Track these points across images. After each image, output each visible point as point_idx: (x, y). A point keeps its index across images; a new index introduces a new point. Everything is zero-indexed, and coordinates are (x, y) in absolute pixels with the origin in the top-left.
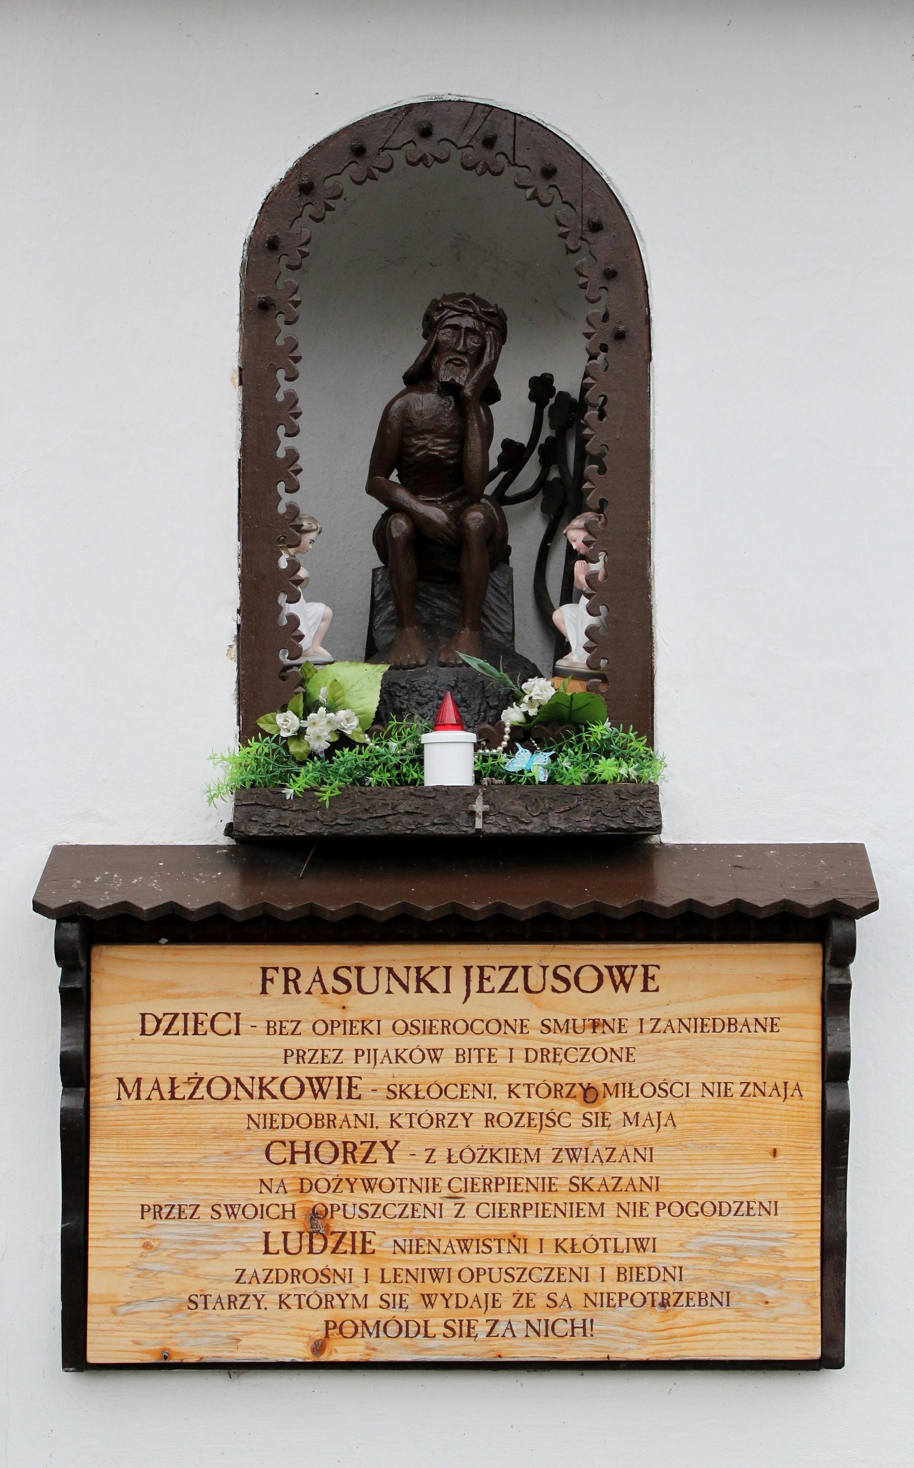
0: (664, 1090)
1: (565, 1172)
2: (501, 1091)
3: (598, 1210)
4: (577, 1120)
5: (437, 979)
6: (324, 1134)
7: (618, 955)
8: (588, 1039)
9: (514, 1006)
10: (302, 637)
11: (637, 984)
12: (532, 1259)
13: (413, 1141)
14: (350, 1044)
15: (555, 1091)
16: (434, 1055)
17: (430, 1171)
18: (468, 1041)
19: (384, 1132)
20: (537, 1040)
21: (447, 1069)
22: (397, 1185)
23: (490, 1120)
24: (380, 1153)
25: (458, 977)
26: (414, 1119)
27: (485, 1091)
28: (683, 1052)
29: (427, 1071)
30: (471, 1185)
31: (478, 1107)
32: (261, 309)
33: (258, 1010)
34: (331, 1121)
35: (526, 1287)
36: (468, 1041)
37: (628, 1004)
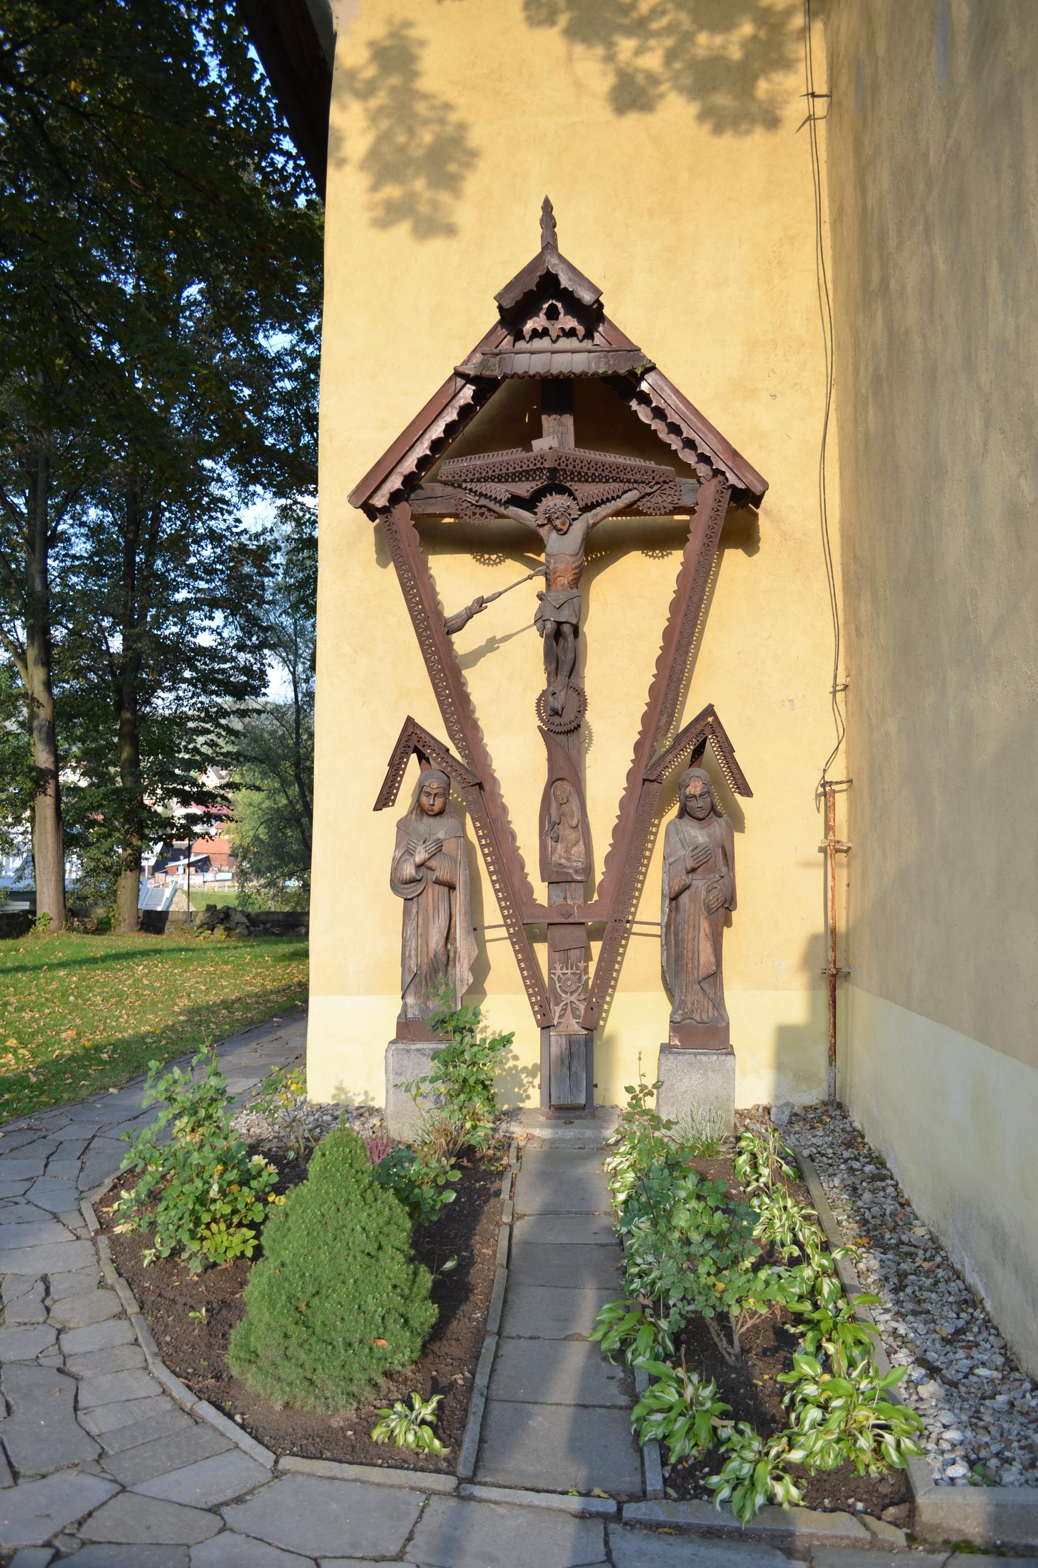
10: (540, 597)
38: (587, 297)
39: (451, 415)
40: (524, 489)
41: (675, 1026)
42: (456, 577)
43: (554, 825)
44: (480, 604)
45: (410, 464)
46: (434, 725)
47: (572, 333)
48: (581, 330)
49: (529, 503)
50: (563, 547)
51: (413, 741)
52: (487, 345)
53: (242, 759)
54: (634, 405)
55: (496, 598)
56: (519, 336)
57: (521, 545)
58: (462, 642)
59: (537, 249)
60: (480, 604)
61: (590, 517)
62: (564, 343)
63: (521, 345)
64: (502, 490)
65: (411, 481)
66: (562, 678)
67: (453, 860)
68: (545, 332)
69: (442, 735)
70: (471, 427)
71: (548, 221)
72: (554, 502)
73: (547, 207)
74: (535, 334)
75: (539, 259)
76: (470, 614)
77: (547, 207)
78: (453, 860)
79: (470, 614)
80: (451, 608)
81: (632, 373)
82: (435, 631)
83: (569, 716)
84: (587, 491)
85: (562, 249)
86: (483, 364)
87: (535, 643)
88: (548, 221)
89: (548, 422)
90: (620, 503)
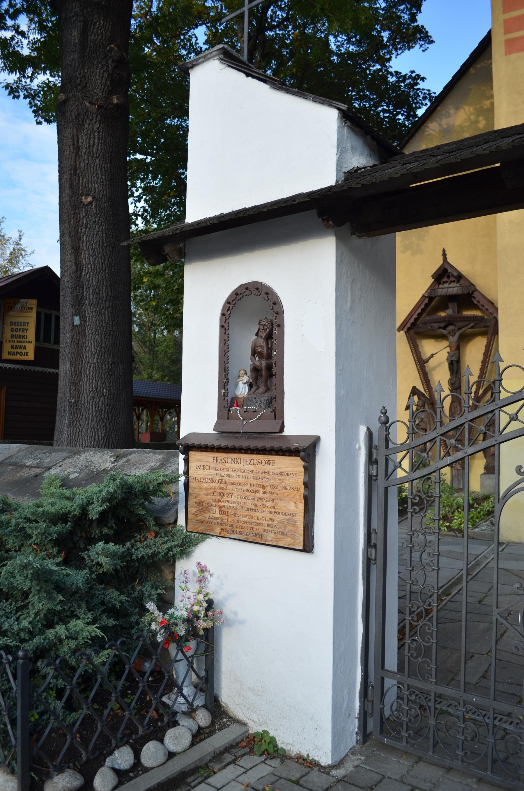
0: (275, 487)
1: (259, 503)
2: (249, 485)
3: (264, 512)
4: (261, 492)
5: (239, 461)
6: (222, 491)
7: (89, 384)
8: (263, 475)
9: (251, 467)
10: (448, 353)
11: (272, 464)
12: (253, 520)
13: (236, 493)
14: (226, 473)
15: (258, 486)
16: (239, 476)
17: (238, 500)
18: (244, 474)
19: (230, 491)
20: (255, 475)
21: (241, 480)
22: (232, 502)
23: (247, 491)
24: (230, 496)
25: (242, 460)
26: (236, 490)
27: (246, 484)
28: (280, 480)
29: (236, 480)
30: (244, 503)
31: (245, 488)
32: (224, 328)
33: (213, 465)
34: (223, 489)
35: (252, 526)
36: (244, 474)
37: (269, 468)
38: (426, 301)
39: (423, 306)
40: (442, 325)
41: (486, 468)
42: (428, 347)
43: (453, 414)
44: (432, 355)
45: (412, 320)
46: (421, 389)
47: (454, 281)
48: (456, 281)
49: (445, 328)
50: (454, 339)
51: (414, 391)
52: (432, 288)
53: (152, 353)
54: (473, 299)
55: (438, 351)
56: (440, 284)
57: (444, 337)
58: (432, 363)
59: (441, 262)
60: (432, 355)
61: (461, 331)
62: (452, 285)
63: (441, 286)
64: (436, 325)
65: (413, 324)
66: (454, 375)
67: (426, 423)
68: (447, 282)
69: (422, 390)
70: (433, 303)
71: (444, 254)
72: (451, 328)
73: (444, 251)
74: (444, 283)
75: (442, 265)
76: (430, 358)
77: (444, 251)
78: (426, 423)
79: (430, 358)
80: (425, 357)
81: (469, 293)
82: (421, 363)
83: (457, 384)
84: (460, 324)
85: (449, 260)
86: (430, 293)
87: (446, 365)
88: (444, 254)
89: (450, 305)
90: (469, 327)
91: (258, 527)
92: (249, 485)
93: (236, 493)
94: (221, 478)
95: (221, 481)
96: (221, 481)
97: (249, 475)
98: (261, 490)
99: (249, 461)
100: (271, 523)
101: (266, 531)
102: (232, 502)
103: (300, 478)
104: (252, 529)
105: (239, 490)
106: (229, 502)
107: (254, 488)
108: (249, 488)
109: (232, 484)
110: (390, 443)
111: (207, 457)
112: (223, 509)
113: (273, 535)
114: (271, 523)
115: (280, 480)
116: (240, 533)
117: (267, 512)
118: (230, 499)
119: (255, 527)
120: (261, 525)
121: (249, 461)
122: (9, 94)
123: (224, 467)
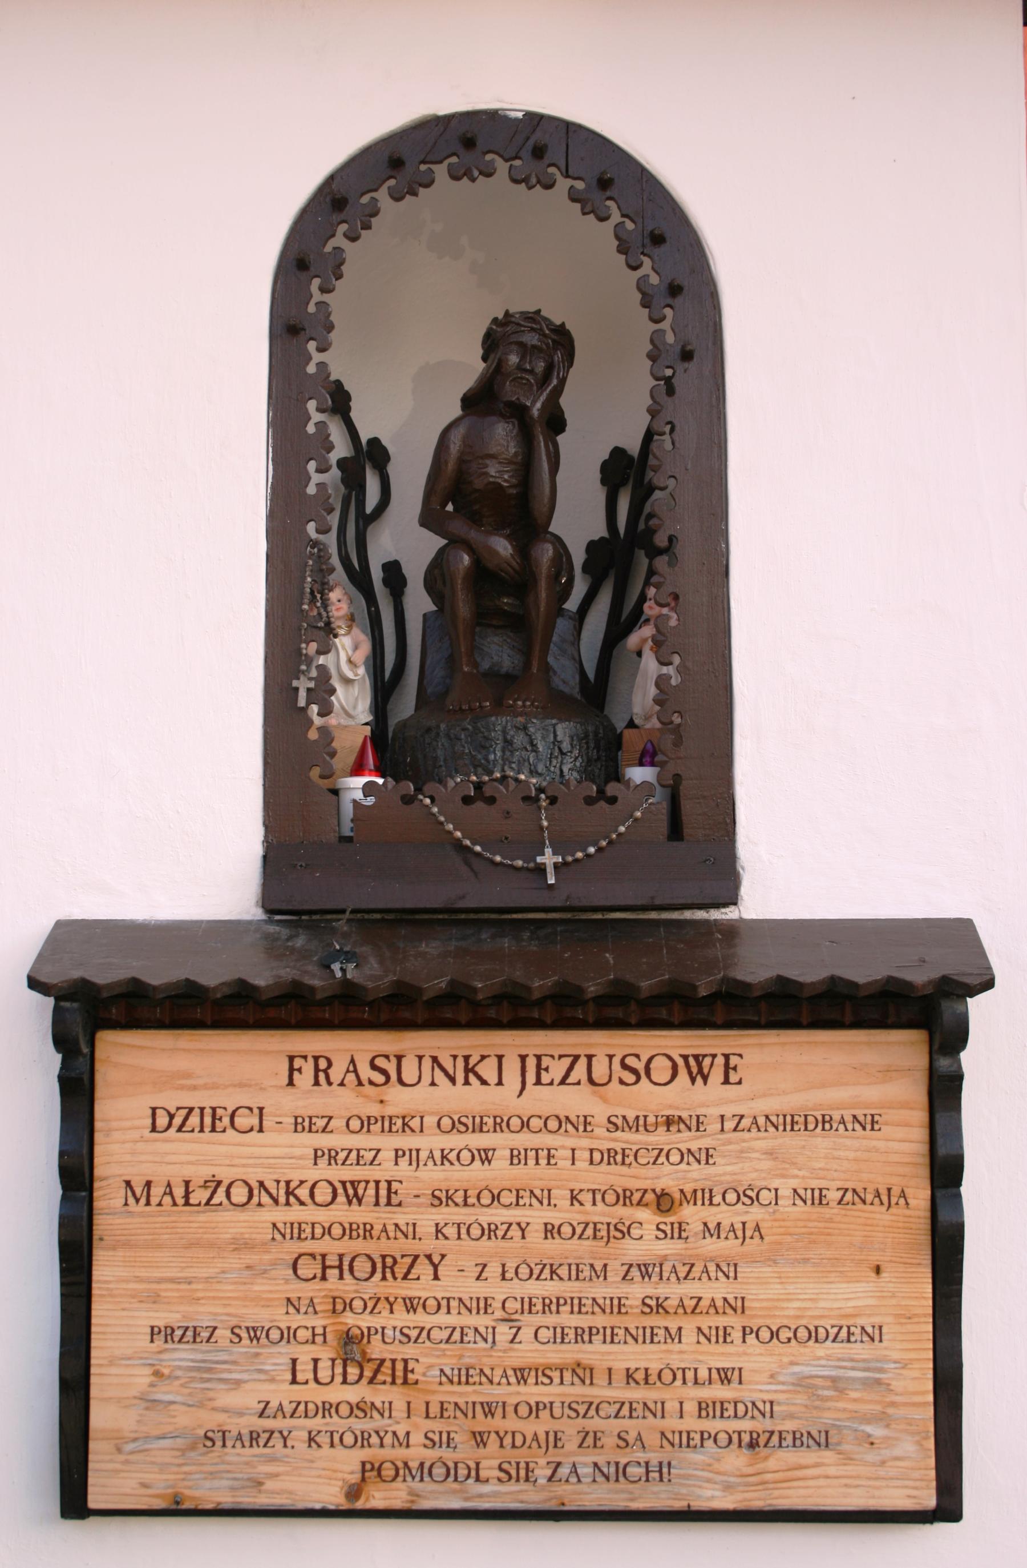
0: (749, 1196)
1: (637, 1291)
2: (560, 1195)
4: (649, 1231)
6: (359, 1246)
8: (660, 1138)
9: (575, 1100)
11: (717, 1075)
12: (600, 1392)
13: (462, 1254)
14: (389, 1143)
15: (624, 1197)
16: (485, 1156)
17: (480, 1290)
18: (524, 1140)
19: (429, 1245)
20: (603, 1140)
22: (443, 1305)
23: (550, 1231)
24: (423, 1269)
27: (545, 1198)
28: (770, 1154)
29: (477, 1173)
30: (528, 1305)
31: (536, 1216)
34: (367, 1232)
35: (594, 1423)
36: (524, 1140)
37: (710, 1098)
73: (519, 1096)
77: (519, 1096)
91: (632, 1427)
92: (560, 1195)
93: (462, 1254)
94: (348, 1173)
95: (352, 1192)
96: (352, 1192)
97: (561, 1142)
98: (646, 1215)
99: (557, 1069)
100: (719, 1392)
101: (687, 1441)
102: (443, 1305)
103: (905, 1139)
104: (590, 1440)
105: (489, 1231)
106: (411, 1305)
107: (601, 1213)
108: (562, 1213)
109: (440, 1199)
110: (651, 456)
111: (240, 1064)
112: (377, 1349)
113: (736, 1460)
114: (719, 1392)
115: (770, 1154)
116: (506, 1475)
117: (689, 1336)
118: (423, 1287)
119: (616, 1425)
120: (655, 1410)
121: (557, 1069)
122: (507, 314)
123: (374, 1110)
